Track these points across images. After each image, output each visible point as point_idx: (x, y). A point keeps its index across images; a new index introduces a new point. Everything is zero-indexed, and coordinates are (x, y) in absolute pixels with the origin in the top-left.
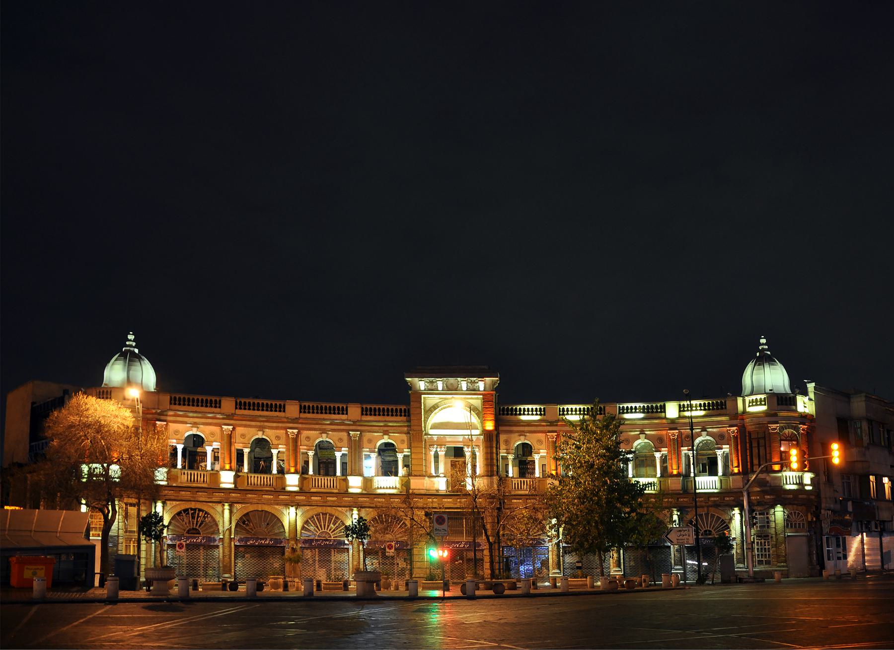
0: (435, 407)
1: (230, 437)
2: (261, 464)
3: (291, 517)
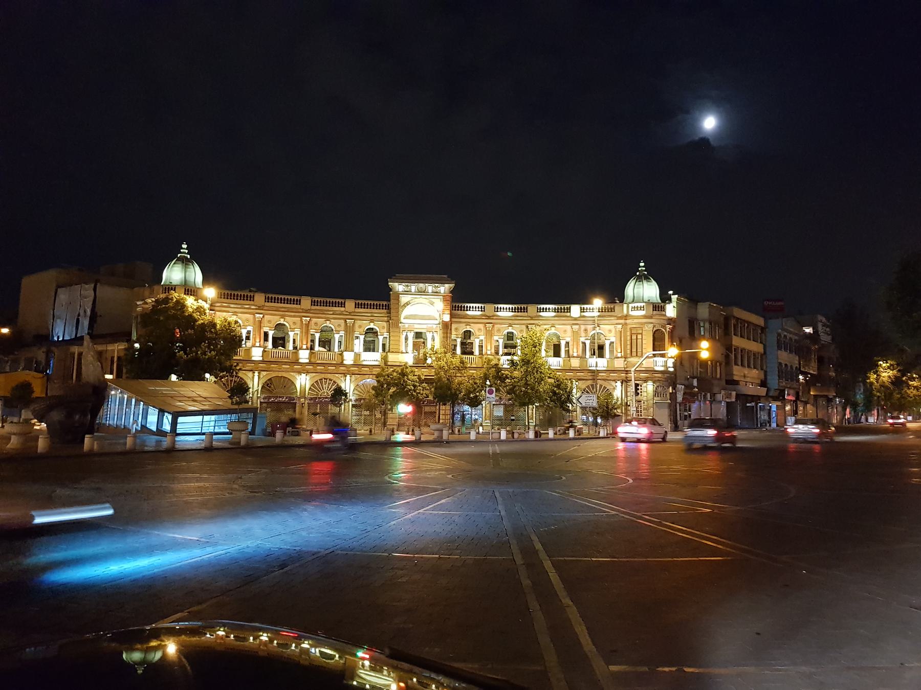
0: (407, 304)
1: (260, 322)
2: (280, 342)
3: (302, 382)
